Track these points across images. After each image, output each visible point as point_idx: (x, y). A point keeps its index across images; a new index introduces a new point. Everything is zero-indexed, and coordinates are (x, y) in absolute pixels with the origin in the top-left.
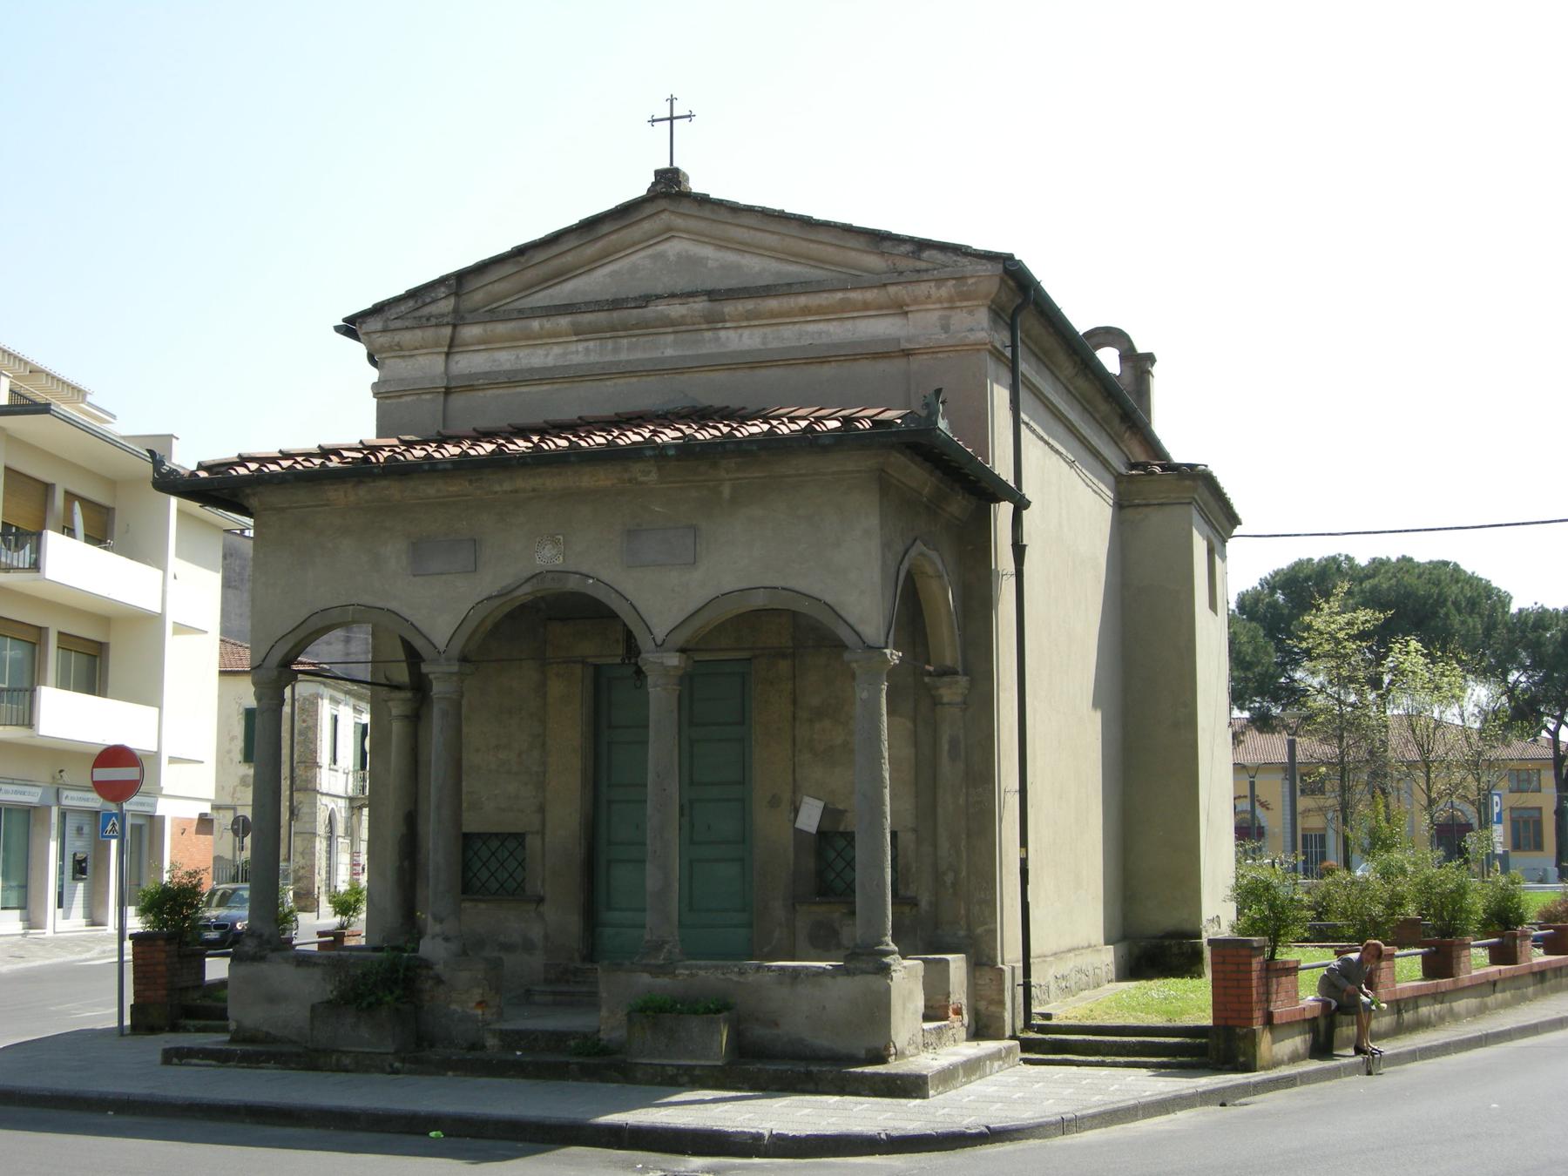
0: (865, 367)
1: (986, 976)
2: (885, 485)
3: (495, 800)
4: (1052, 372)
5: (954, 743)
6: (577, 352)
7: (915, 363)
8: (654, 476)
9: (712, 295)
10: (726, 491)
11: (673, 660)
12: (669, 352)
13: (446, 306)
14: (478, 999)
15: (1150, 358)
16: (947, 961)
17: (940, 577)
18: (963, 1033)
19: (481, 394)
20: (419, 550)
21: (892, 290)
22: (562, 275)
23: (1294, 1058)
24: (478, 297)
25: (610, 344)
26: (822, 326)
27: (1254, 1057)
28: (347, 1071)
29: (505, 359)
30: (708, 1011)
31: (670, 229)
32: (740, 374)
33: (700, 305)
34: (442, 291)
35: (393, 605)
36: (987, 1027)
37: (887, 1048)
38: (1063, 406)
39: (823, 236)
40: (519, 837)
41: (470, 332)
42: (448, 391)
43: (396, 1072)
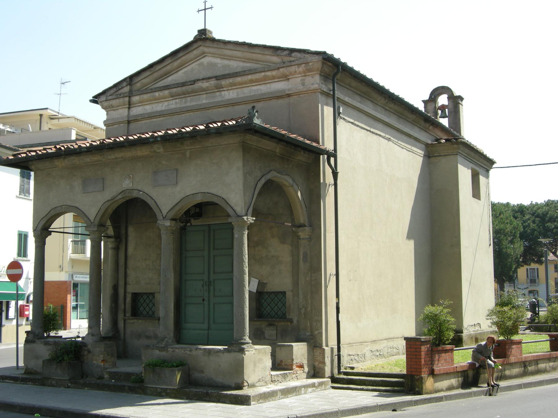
0: (274, 102)
1: (317, 352)
2: (246, 149)
3: (140, 279)
4: (372, 102)
5: (305, 255)
6: (173, 104)
7: (292, 99)
8: (161, 150)
9: (218, 78)
10: (188, 154)
11: (168, 223)
12: (204, 101)
13: (126, 89)
14: (102, 359)
15: (461, 98)
16: (292, 346)
17: (292, 186)
18: (305, 375)
19: (140, 122)
20: (85, 182)
21: (281, 70)
22: (168, 74)
23: (450, 388)
24: (138, 85)
25: (184, 100)
26: (259, 87)
27: (422, 388)
28: (53, 386)
29: (148, 109)
30: (173, 366)
31: (204, 53)
32: (229, 108)
33: (213, 82)
34: (125, 84)
35: (77, 205)
36: (318, 373)
37: (243, 383)
38: (379, 115)
39: (257, 50)
40: (153, 294)
41: (135, 99)
42: (129, 122)
43: (69, 387)
